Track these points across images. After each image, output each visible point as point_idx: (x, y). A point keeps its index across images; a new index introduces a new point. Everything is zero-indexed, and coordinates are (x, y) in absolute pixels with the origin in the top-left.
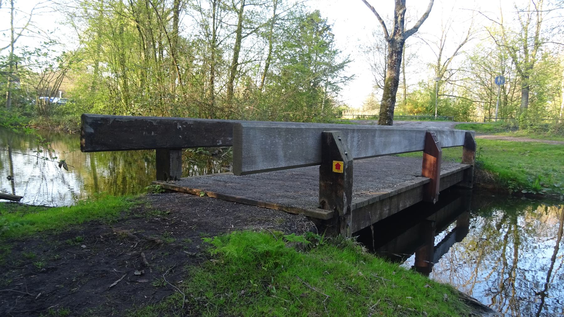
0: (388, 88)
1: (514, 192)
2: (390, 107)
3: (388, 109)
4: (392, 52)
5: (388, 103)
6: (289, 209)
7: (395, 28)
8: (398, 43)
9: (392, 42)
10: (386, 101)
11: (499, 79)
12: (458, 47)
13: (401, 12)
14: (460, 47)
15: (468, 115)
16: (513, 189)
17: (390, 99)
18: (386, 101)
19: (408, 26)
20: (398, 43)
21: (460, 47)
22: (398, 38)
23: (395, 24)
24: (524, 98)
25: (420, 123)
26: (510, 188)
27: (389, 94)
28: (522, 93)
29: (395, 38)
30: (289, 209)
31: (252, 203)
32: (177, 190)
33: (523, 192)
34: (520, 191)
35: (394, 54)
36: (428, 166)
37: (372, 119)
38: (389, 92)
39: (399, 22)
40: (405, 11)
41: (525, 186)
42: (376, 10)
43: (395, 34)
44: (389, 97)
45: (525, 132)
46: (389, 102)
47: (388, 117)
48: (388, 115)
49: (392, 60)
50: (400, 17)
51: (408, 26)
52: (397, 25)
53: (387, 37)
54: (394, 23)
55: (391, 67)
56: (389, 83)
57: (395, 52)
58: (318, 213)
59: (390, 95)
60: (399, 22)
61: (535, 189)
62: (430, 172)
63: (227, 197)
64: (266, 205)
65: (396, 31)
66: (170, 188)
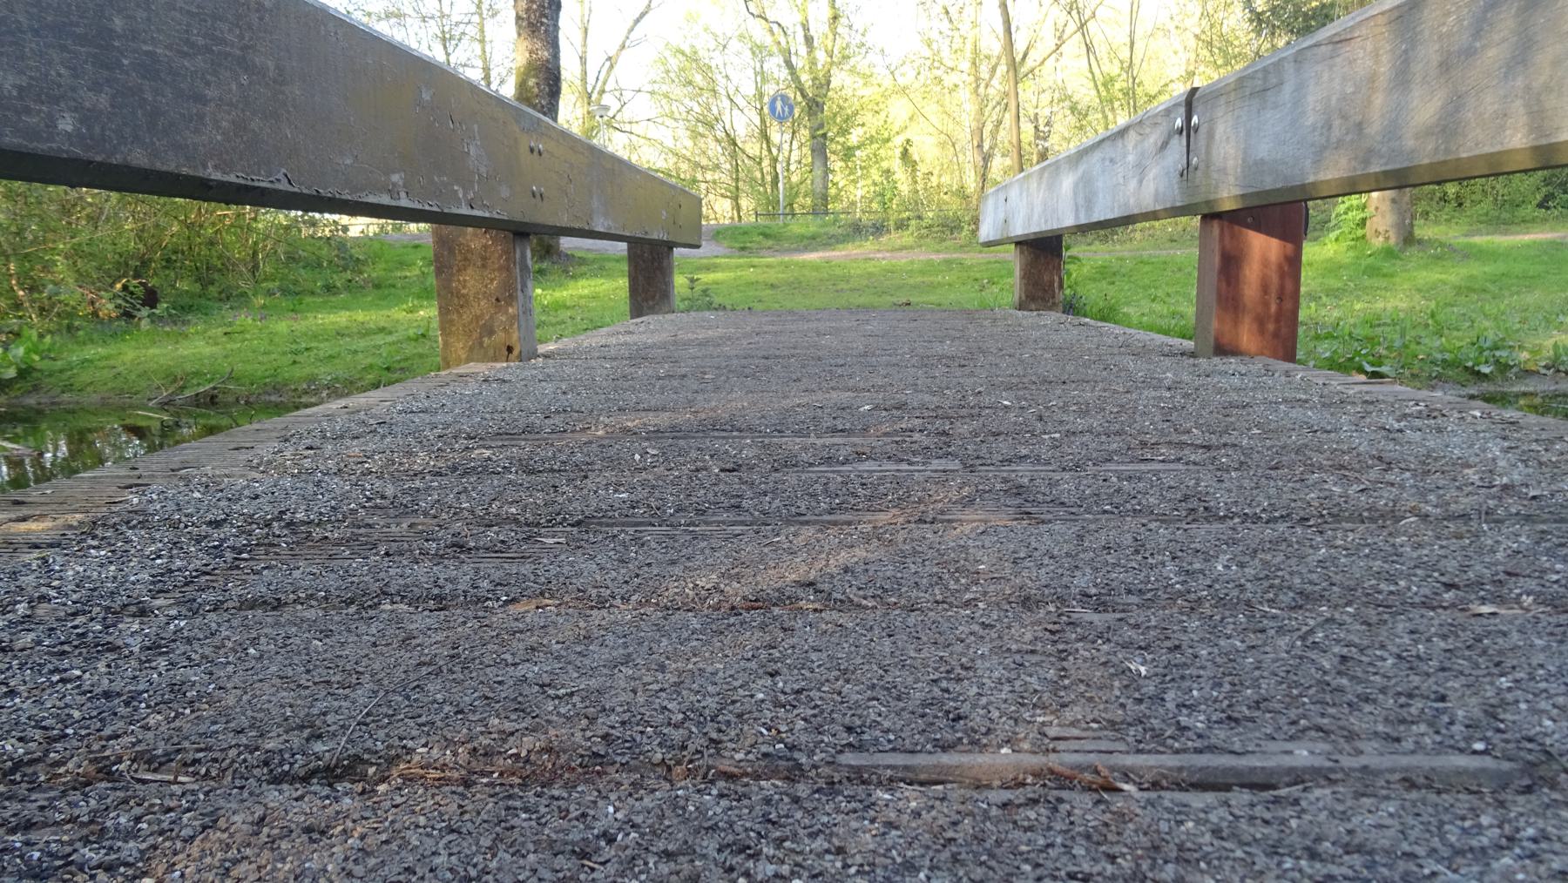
11: (779, 104)
14: (637, 21)
21: (637, 21)
24: (818, 163)
45: (907, 238)
56: (531, 82)
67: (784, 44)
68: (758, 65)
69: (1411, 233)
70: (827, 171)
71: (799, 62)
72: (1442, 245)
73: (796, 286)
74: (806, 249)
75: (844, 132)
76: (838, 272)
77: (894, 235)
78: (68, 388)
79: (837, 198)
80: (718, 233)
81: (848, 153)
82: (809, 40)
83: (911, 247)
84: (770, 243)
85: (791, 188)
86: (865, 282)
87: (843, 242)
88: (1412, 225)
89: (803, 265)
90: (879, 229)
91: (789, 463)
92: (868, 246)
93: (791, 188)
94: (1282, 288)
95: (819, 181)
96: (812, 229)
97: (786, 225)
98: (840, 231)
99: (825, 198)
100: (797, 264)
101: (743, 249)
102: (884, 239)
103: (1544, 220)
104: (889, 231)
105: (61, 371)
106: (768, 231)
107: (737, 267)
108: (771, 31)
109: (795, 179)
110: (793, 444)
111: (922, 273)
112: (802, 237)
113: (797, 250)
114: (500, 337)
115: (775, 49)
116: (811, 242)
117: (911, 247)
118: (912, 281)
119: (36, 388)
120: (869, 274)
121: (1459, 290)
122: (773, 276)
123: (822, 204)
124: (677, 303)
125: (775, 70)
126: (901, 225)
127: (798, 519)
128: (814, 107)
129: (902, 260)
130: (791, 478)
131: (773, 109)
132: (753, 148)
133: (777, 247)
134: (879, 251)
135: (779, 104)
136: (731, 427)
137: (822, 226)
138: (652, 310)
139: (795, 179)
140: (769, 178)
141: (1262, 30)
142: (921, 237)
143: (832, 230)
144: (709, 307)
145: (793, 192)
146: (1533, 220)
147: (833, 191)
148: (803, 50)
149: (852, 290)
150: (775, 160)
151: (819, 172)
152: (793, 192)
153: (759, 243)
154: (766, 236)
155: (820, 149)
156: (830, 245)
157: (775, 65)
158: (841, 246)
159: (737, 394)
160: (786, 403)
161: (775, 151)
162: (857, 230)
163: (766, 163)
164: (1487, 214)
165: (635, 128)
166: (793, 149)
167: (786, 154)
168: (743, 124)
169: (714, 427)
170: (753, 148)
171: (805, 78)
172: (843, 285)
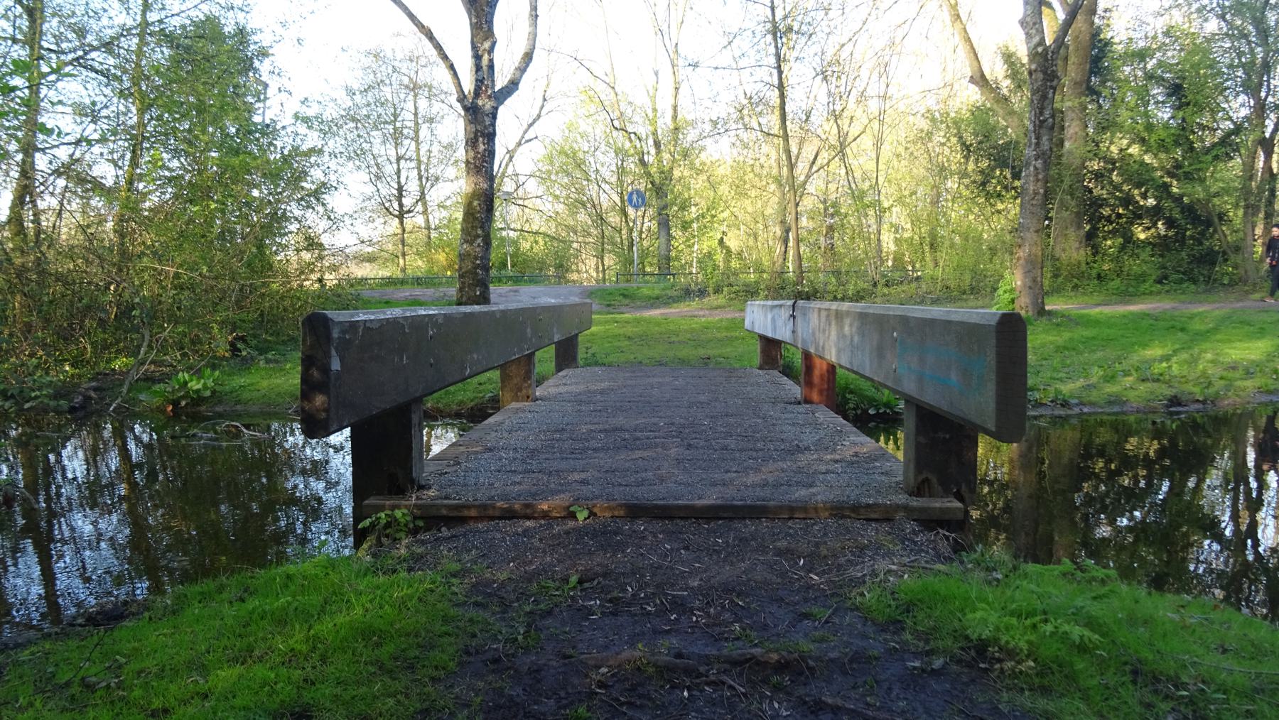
0: (472, 214)
1: (856, 414)
2: (482, 258)
3: (478, 262)
4: (476, 133)
5: (478, 249)
6: (862, 511)
7: (477, 80)
8: (487, 115)
9: (474, 112)
10: (472, 244)
11: (635, 197)
12: (525, 126)
13: (487, 45)
14: (530, 125)
15: (567, 270)
16: (854, 409)
17: (479, 240)
18: (472, 244)
19: (500, 82)
20: (487, 115)
21: (530, 125)
22: (485, 103)
23: (477, 72)
24: (663, 233)
25: (516, 291)
26: (850, 408)
27: (476, 227)
28: (659, 224)
29: (480, 103)
30: (862, 511)
31: (755, 512)
32: (473, 513)
33: (872, 412)
34: (865, 411)
35: (481, 139)
36: (816, 380)
37: (382, 285)
38: (477, 223)
39: (485, 68)
40: (494, 44)
41: (872, 402)
42: (435, 34)
43: (477, 94)
44: (478, 236)
45: (720, 300)
46: (479, 245)
47: (478, 281)
48: (480, 277)
49: (478, 153)
50: (486, 57)
51: (500, 82)
52: (479, 73)
53: (462, 98)
54: (474, 69)
55: (476, 167)
56: (476, 203)
57: (483, 135)
58: (940, 508)
59: (480, 232)
60: (485, 68)
61: (887, 405)
62: (821, 392)
63: (657, 507)
64: (792, 511)
65: (481, 89)
66: (444, 512)
67: (638, 146)
68: (620, 163)
69: (1043, 308)
70: (670, 237)
71: (650, 159)
72: (1063, 316)
73: (643, 339)
74: (653, 306)
75: (683, 208)
76: (672, 327)
77: (713, 297)
78: (238, 402)
79: (677, 259)
80: (592, 293)
81: (685, 226)
82: (657, 144)
83: (724, 307)
84: (627, 301)
85: (643, 251)
86: (689, 336)
87: (674, 302)
88: (1043, 303)
89: (648, 321)
90: (702, 293)
91: (638, 439)
92: (690, 306)
93: (643, 251)
94: (829, 378)
95: (663, 247)
96: (657, 292)
97: (638, 288)
98: (676, 293)
99: (668, 259)
100: (645, 320)
101: (609, 305)
102: (705, 300)
103: (1159, 293)
104: (709, 295)
105: (231, 392)
106: (626, 293)
107: (606, 322)
108: (630, 138)
109: (646, 244)
110: (639, 434)
111: (727, 329)
112: (650, 298)
113: (647, 308)
114: (524, 391)
115: (632, 151)
116: (655, 302)
117: (724, 307)
118: (719, 335)
119: (220, 402)
120: (693, 329)
121: (1058, 349)
122: (630, 330)
123: (666, 261)
124: (581, 362)
125: (632, 166)
126: (718, 290)
127: (639, 449)
128: (659, 190)
129: (716, 317)
130: (638, 442)
131: (630, 201)
132: (614, 219)
133: (632, 305)
134: (702, 309)
135: (635, 197)
136: (622, 430)
137: (663, 289)
138: (568, 366)
139: (646, 244)
140: (626, 243)
141: (970, 156)
142: (731, 299)
143: (670, 293)
144: (596, 364)
145: (644, 254)
146: (1151, 293)
147: (673, 254)
148: (653, 151)
149: (679, 342)
150: (631, 230)
151: (663, 240)
152: (644, 254)
153: (620, 301)
154: (625, 296)
155: (664, 224)
156: (669, 304)
157: (631, 165)
158: (675, 305)
159: (621, 418)
160: (637, 422)
161: (631, 224)
162: (687, 293)
163: (624, 232)
164: (1118, 288)
165: (526, 203)
166: (645, 221)
167: (639, 226)
168: (608, 198)
169: (615, 430)
170: (614, 219)
171: (653, 170)
172: (674, 339)
